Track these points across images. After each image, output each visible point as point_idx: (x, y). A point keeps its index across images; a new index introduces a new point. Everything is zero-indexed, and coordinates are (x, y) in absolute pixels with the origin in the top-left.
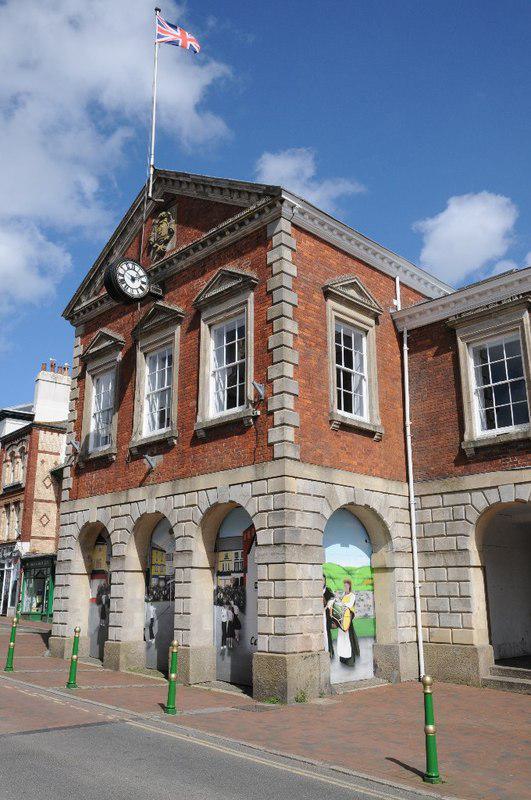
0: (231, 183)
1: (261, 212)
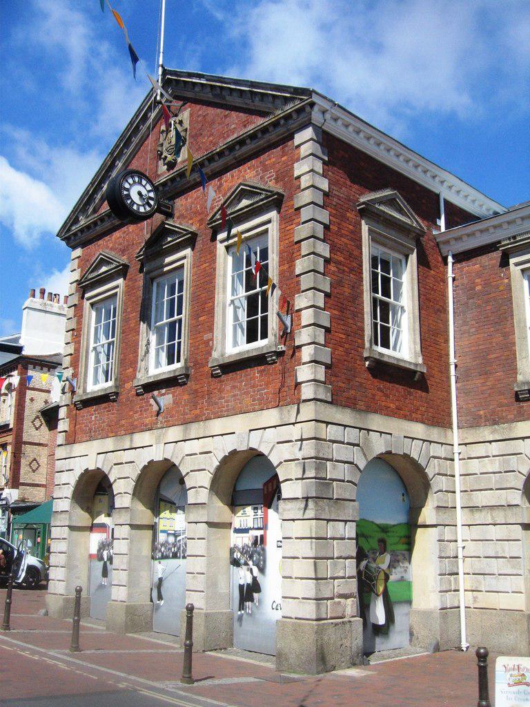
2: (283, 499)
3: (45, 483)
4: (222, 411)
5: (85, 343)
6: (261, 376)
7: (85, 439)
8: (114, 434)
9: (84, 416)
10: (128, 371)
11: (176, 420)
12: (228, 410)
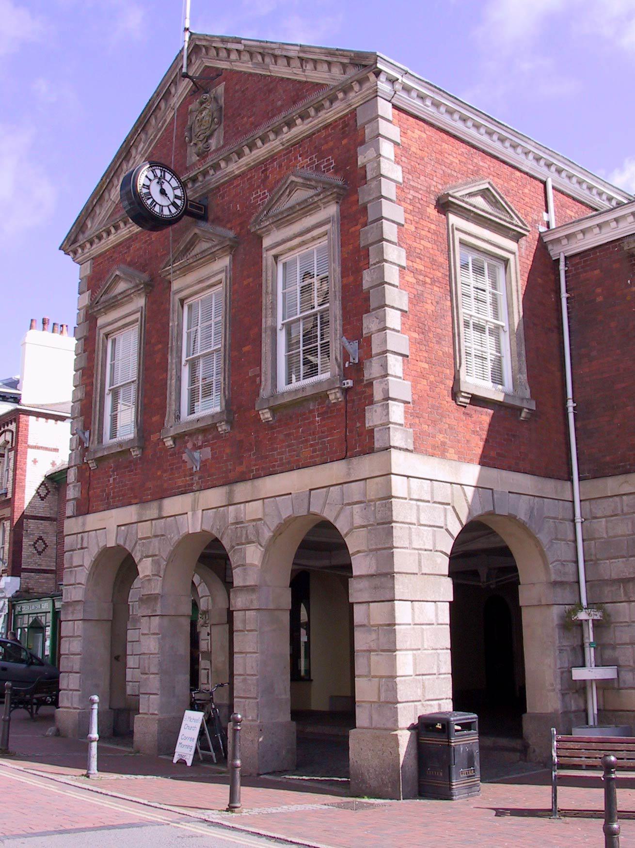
3: (54, 568)
4: (274, 466)
7: (101, 508)
12: (281, 465)
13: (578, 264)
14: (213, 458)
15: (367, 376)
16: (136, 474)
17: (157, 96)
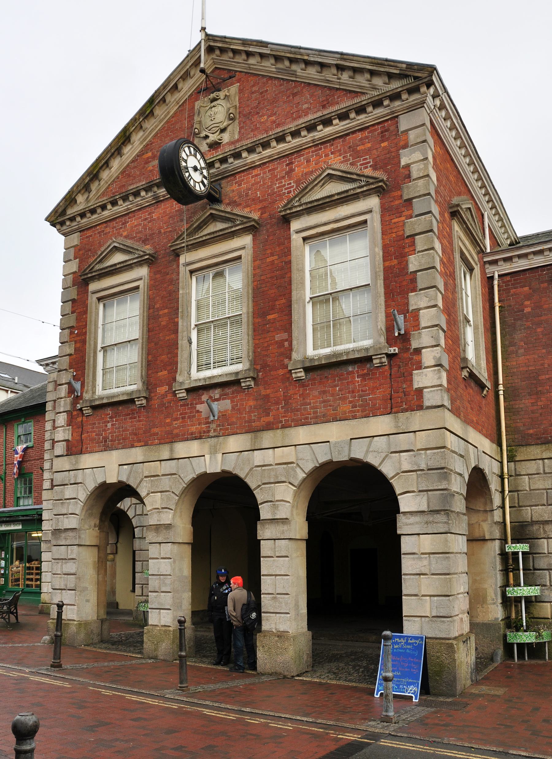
0: (343, 55)
1: (395, 96)
2: (402, 513)
4: (307, 418)
5: (92, 343)
6: (364, 380)
8: (143, 444)
9: (95, 424)
10: (160, 374)
11: (237, 428)
12: (316, 417)
13: (509, 281)
14: (233, 408)
15: (415, 344)
16: (140, 421)
17: (164, 88)
